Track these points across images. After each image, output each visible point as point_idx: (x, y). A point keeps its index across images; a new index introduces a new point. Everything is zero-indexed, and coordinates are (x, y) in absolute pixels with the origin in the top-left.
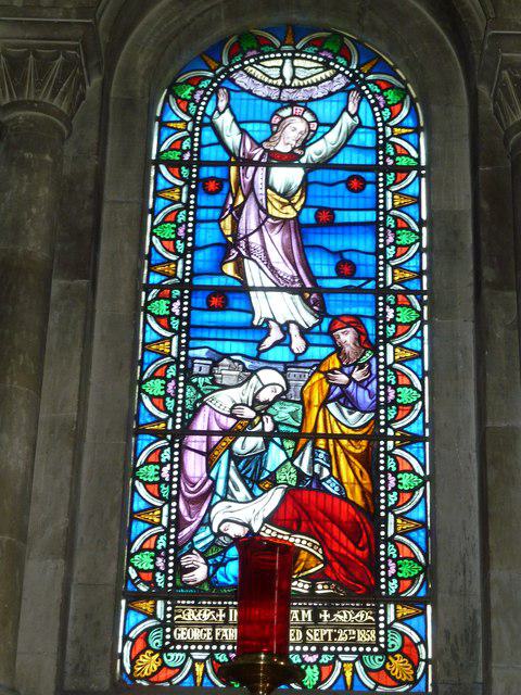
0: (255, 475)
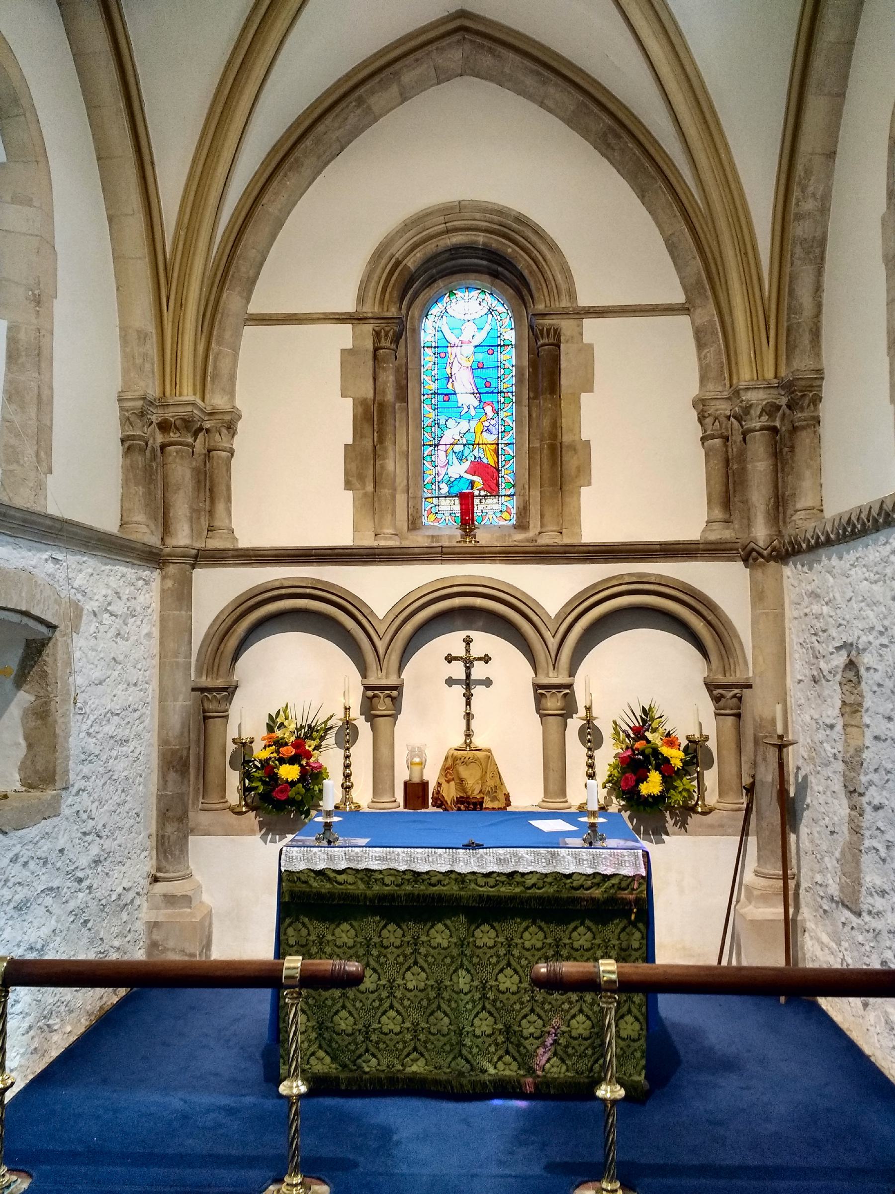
0: (461, 459)
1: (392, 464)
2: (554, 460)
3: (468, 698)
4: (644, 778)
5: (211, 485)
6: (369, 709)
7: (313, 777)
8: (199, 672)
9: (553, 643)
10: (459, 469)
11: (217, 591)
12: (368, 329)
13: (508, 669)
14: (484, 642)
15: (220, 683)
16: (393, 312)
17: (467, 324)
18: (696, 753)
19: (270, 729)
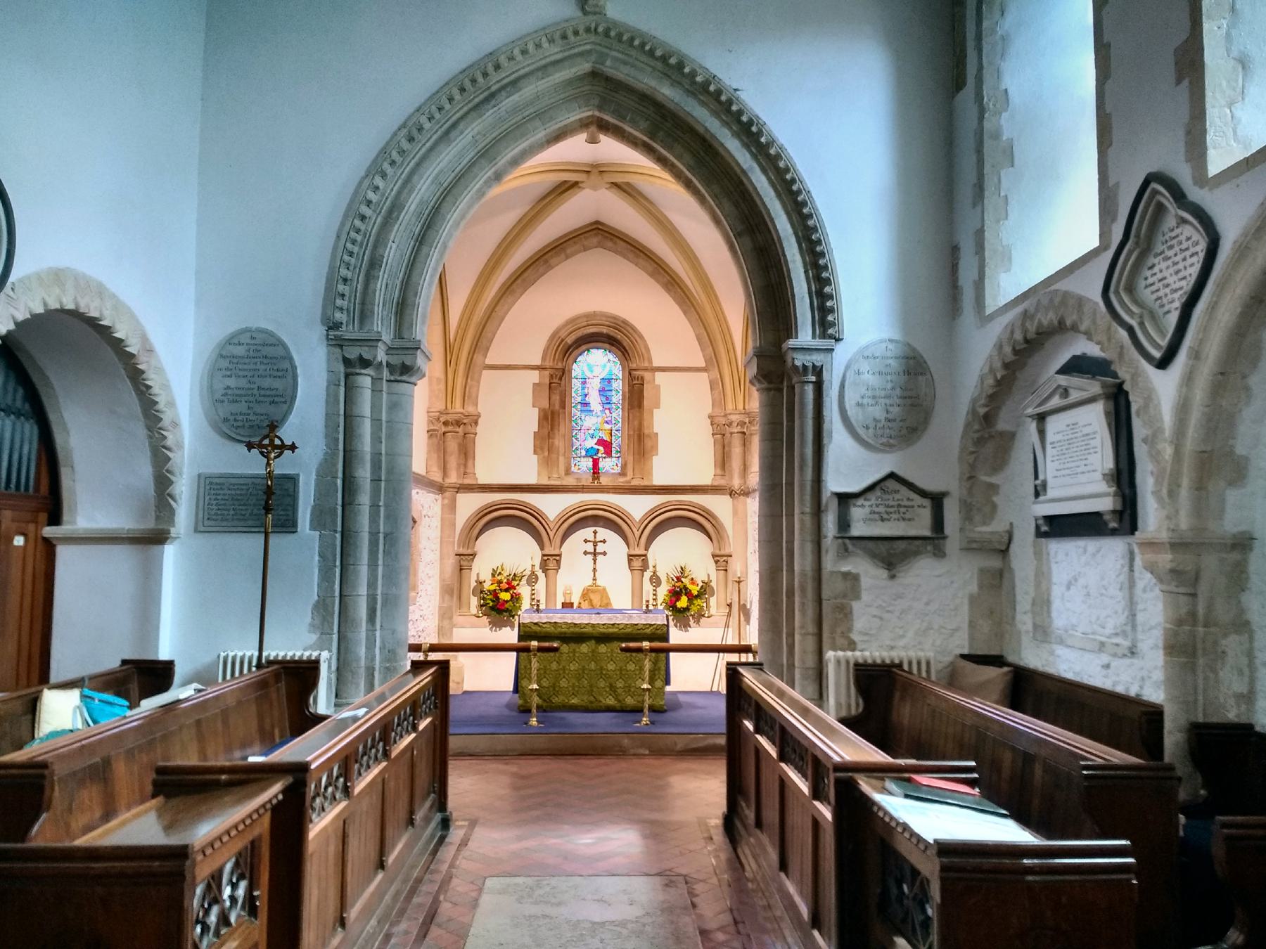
0: (592, 436)
1: (558, 442)
2: (641, 443)
3: (595, 561)
4: (678, 599)
5: (466, 452)
6: (544, 567)
7: (516, 598)
8: (459, 546)
9: (637, 534)
10: (591, 443)
11: (469, 504)
12: (547, 373)
13: (613, 544)
14: (603, 533)
15: (469, 552)
16: (560, 366)
17: (596, 366)
18: (705, 590)
19: (493, 575)
